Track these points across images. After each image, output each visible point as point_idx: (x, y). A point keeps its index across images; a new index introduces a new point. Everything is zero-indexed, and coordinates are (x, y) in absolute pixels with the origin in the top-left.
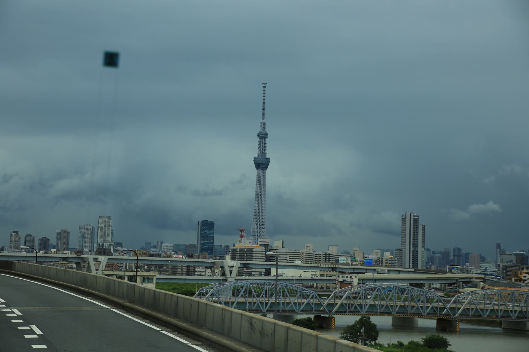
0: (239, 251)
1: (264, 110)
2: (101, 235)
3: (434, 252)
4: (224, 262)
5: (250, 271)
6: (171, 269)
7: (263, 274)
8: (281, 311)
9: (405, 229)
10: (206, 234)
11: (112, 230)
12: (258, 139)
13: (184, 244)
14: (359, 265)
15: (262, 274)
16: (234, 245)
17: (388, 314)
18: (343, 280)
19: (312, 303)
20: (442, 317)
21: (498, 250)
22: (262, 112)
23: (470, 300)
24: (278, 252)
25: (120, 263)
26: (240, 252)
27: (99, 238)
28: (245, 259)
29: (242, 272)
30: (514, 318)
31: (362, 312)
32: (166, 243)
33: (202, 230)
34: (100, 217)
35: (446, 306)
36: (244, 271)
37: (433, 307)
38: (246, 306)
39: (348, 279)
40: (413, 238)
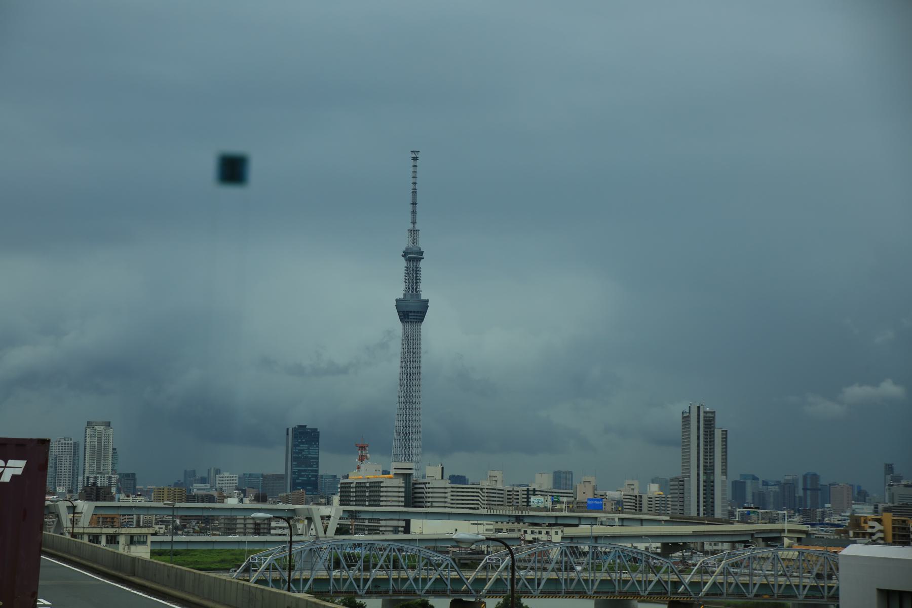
0: (356, 487)
1: (414, 204)
2: (92, 459)
3: (765, 483)
4: (313, 510)
5: (376, 526)
6: (225, 524)
7: (401, 531)
8: (391, 593)
9: (689, 438)
10: (303, 453)
11: (114, 449)
12: (403, 263)
13: (261, 473)
14: (565, 510)
15: (399, 531)
16: (347, 477)
17: (579, 595)
18: (533, 538)
19: (447, 579)
20: (675, 599)
21: (889, 477)
22: (410, 208)
23: (724, 568)
24: (429, 488)
25: (128, 515)
26: (358, 489)
27: (87, 465)
28: (367, 503)
29: (362, 527)
30: (801, 598)
31: (534, 591)
32: (224, 473)
33: (294, 446)
34: (89, 424)
35: (682, 580)
36: (366, 526)
37: (661, 581)
38: (329, 585)
39: (543, 537)
40: (705, 456)
